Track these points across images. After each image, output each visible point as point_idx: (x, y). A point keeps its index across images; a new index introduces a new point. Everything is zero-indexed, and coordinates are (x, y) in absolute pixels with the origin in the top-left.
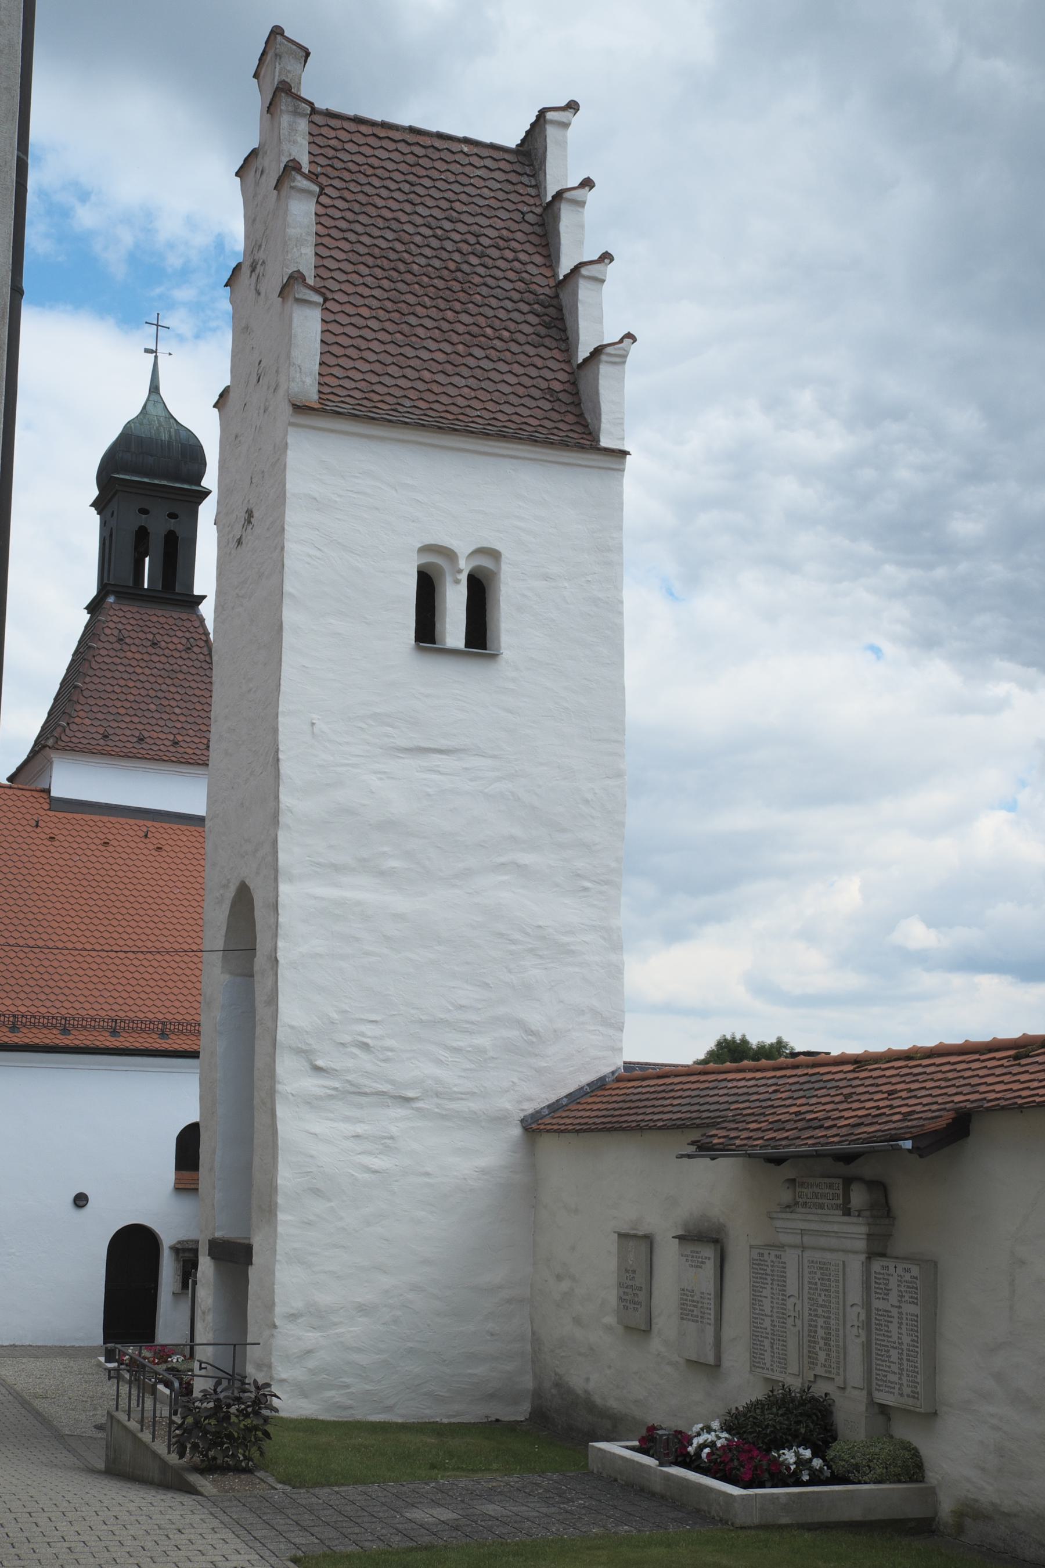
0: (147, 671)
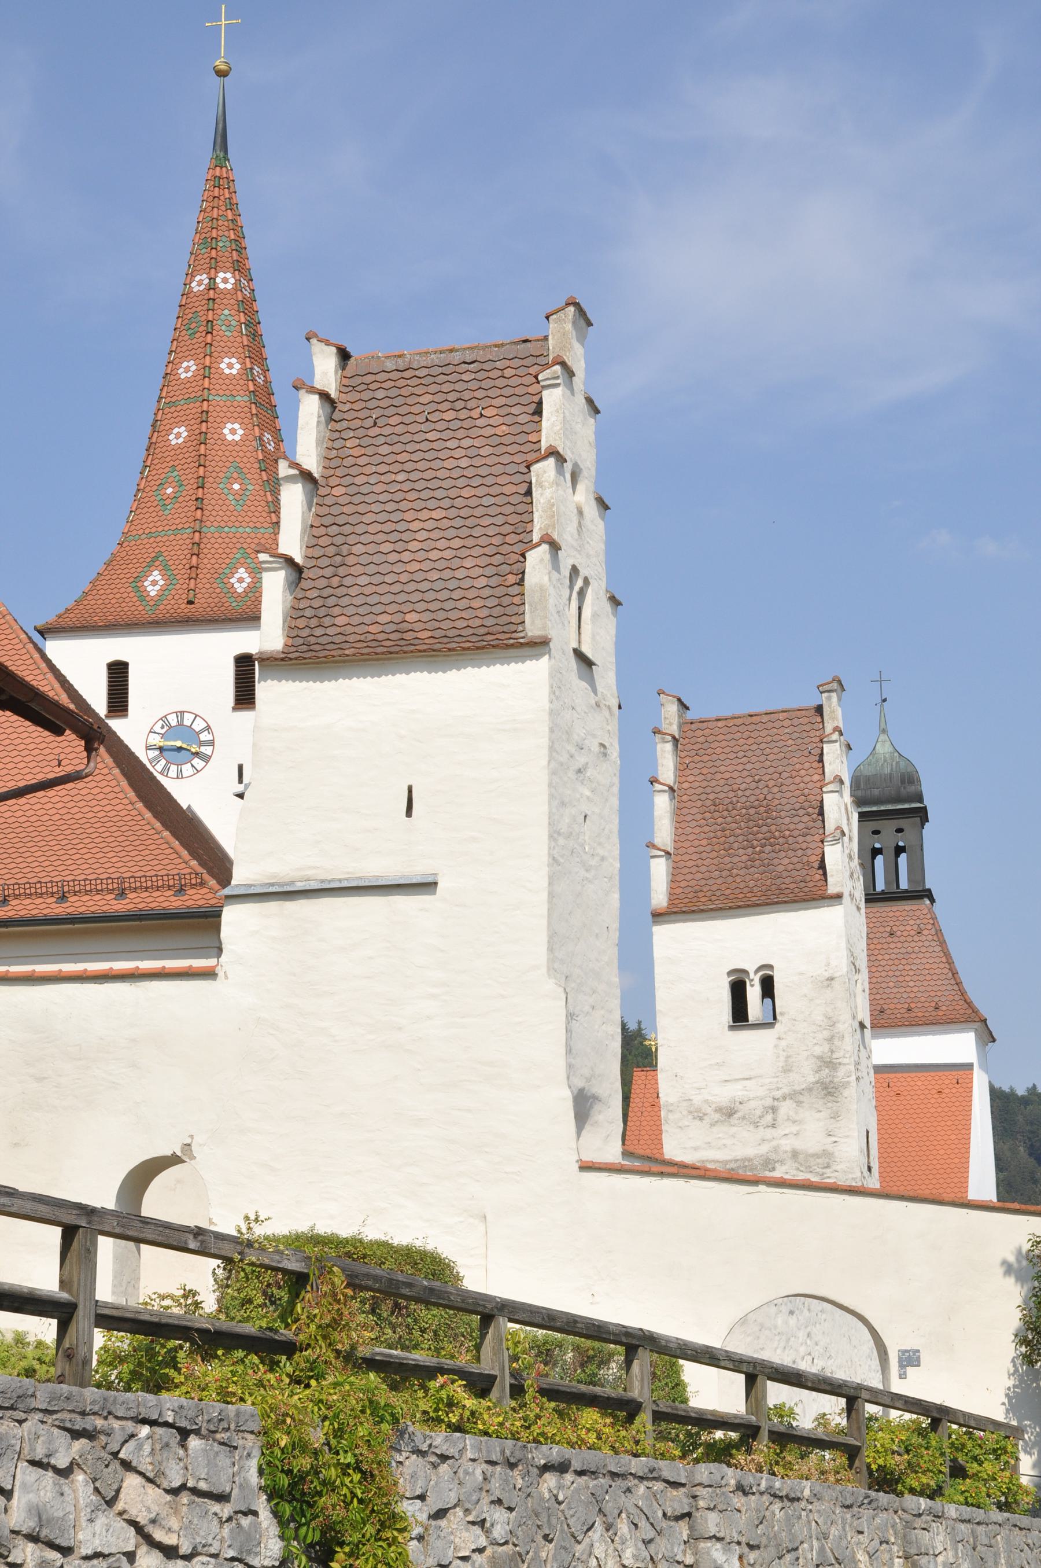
0: (887, 957)
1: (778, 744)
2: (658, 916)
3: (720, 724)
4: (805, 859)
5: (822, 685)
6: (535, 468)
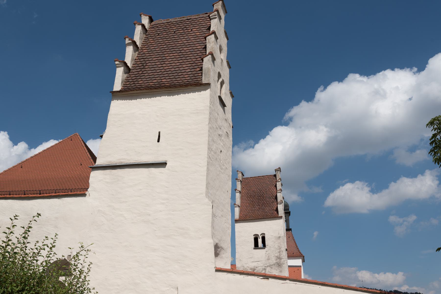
1: (265, 183)
2: (237, 221)
3: (251, 179)
4: (273, 208)
5: (276, 169)
6: (207, 38)
